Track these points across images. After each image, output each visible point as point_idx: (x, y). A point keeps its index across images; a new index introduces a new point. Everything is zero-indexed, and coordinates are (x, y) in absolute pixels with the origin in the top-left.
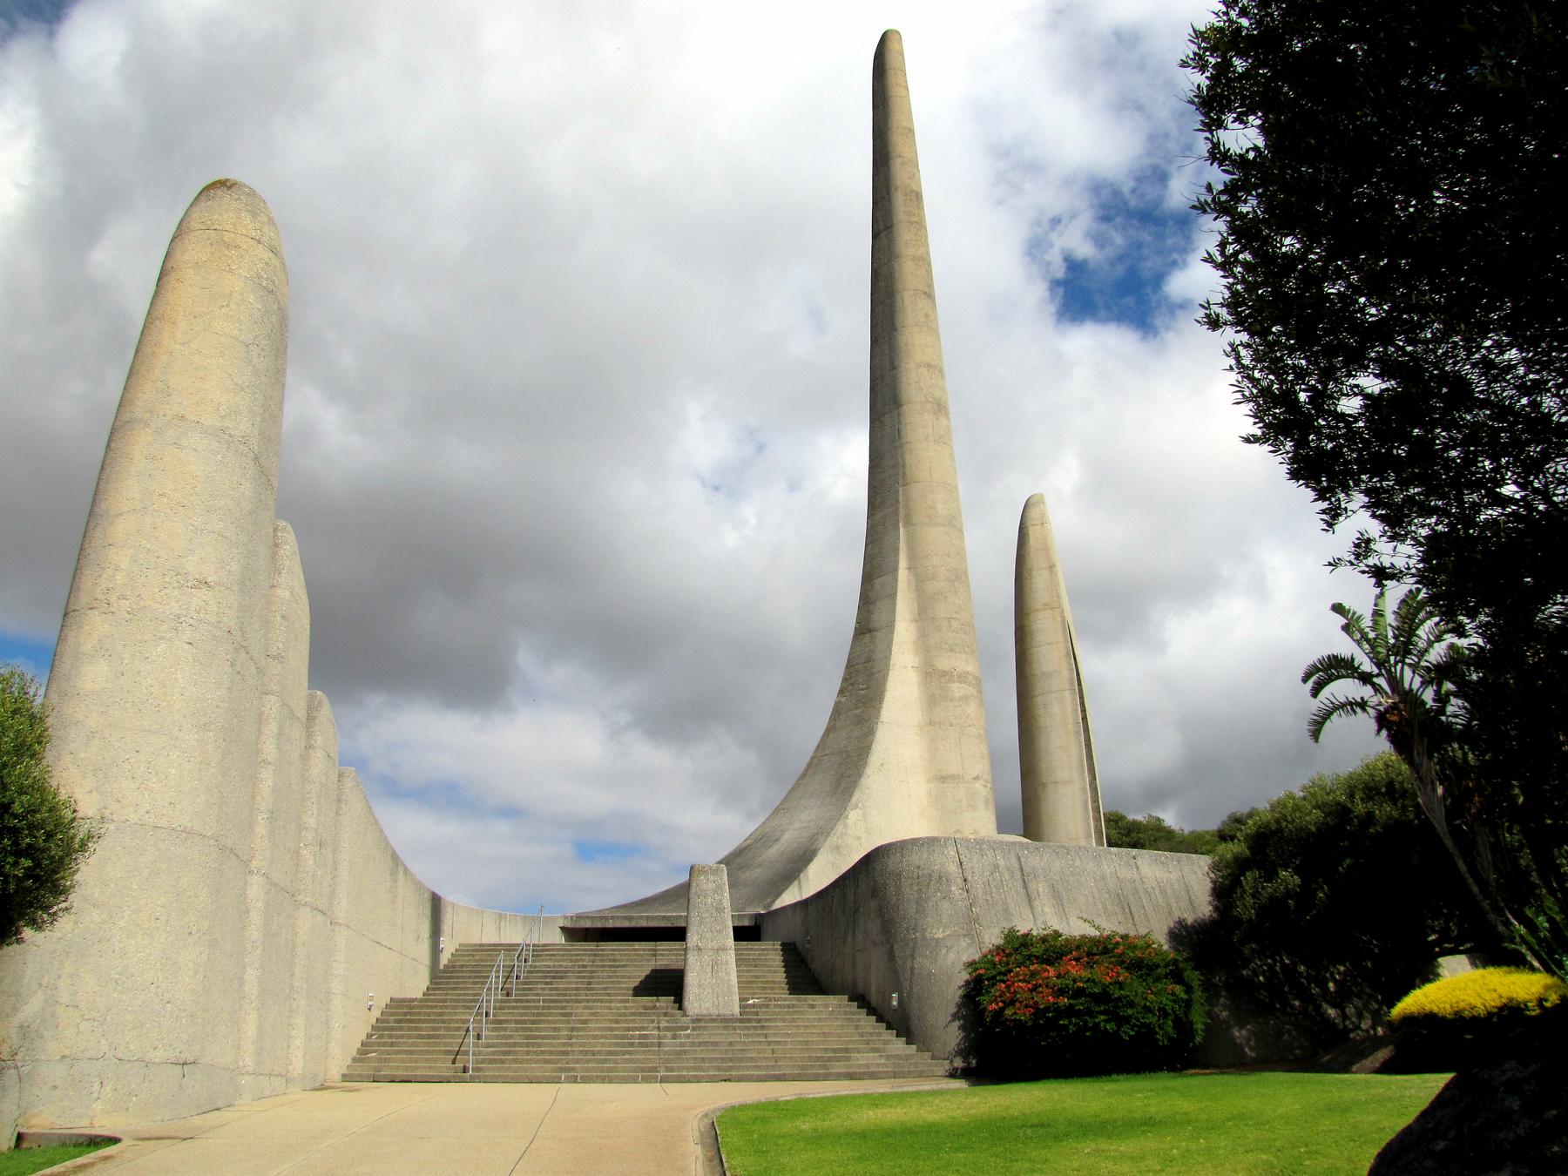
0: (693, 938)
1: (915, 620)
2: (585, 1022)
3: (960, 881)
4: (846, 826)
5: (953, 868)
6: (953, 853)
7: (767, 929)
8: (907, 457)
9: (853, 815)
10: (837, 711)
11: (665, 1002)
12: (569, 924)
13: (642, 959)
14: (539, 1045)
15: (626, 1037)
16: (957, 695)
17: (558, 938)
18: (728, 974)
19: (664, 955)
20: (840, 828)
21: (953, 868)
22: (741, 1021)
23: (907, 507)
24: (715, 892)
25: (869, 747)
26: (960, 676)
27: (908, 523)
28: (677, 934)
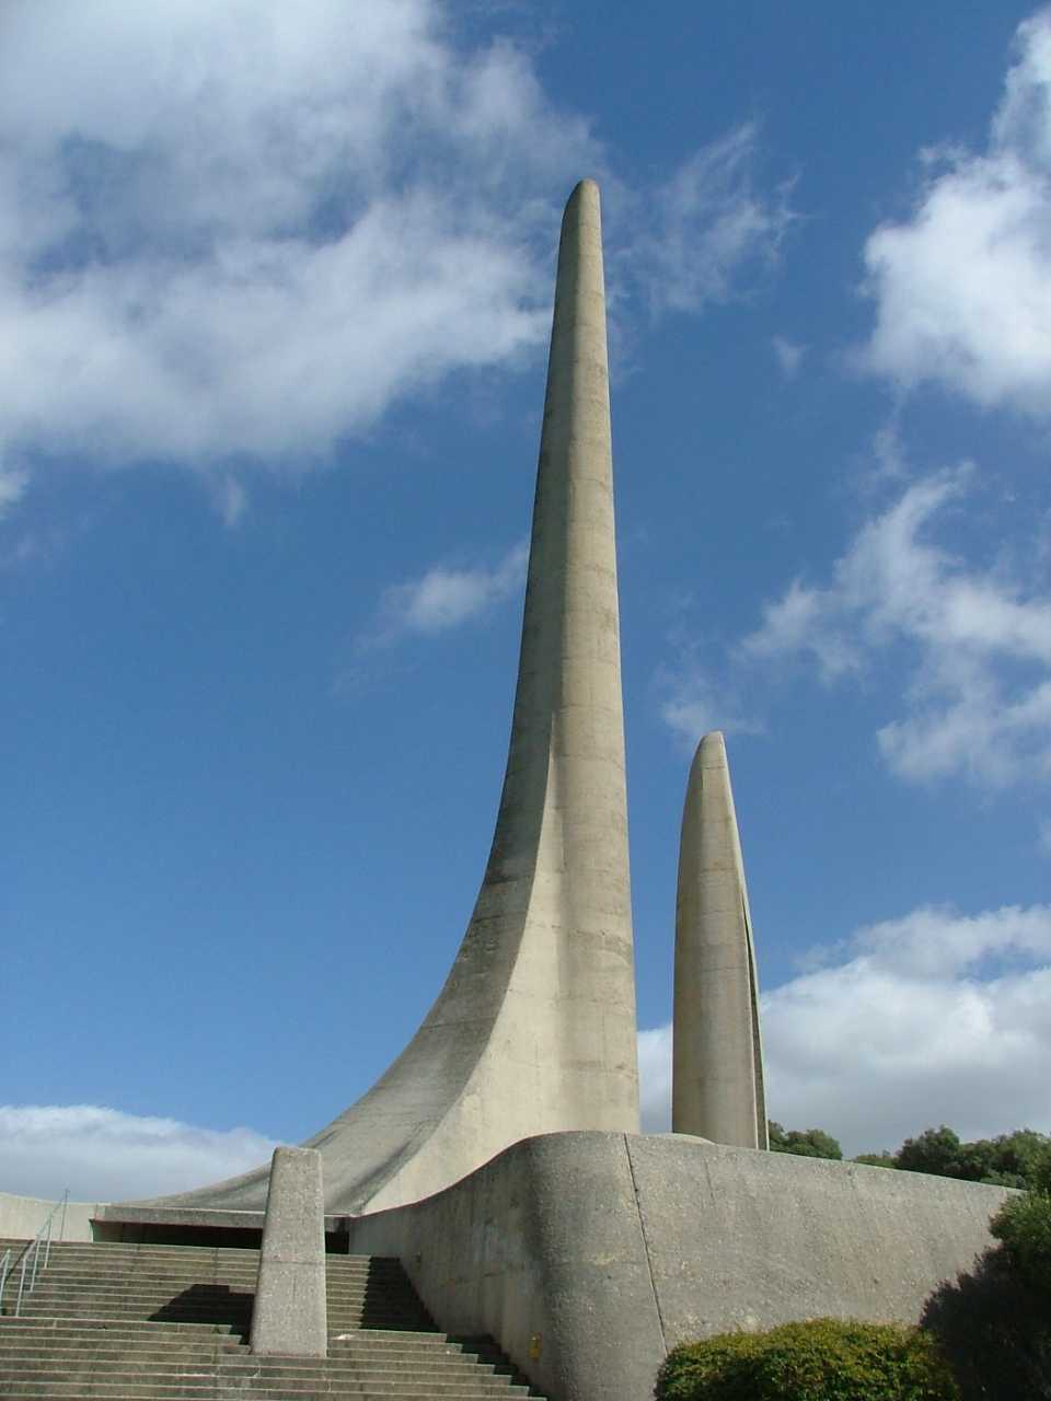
0: (271, 1245)
1: (559, 871)
2: (115, 1356)
3: (630, 1191)
4: (459, 1112)
5: (622, 1174)
6: (622, 1153)
7: (356, 1240)
8: (565, 675)
9: (468, 1102)
10: (457, 972)
11: (226, 1336)
12: (101, 1217)
13: (192, 1266)
14: (32, 1343)
15: (168, 1380)
16: (604, 965)
17: (85, 1235)
18: (315, 1297)
19: (227, 1267)
20: (451, 1116)
21: (622, 1174)
22: (328, 1364)
23: (560, 736)
24: (305, 1186)
25: (493, 1020)
26: (608, 942)
27: (561, 752)
28: (250, 1238)
